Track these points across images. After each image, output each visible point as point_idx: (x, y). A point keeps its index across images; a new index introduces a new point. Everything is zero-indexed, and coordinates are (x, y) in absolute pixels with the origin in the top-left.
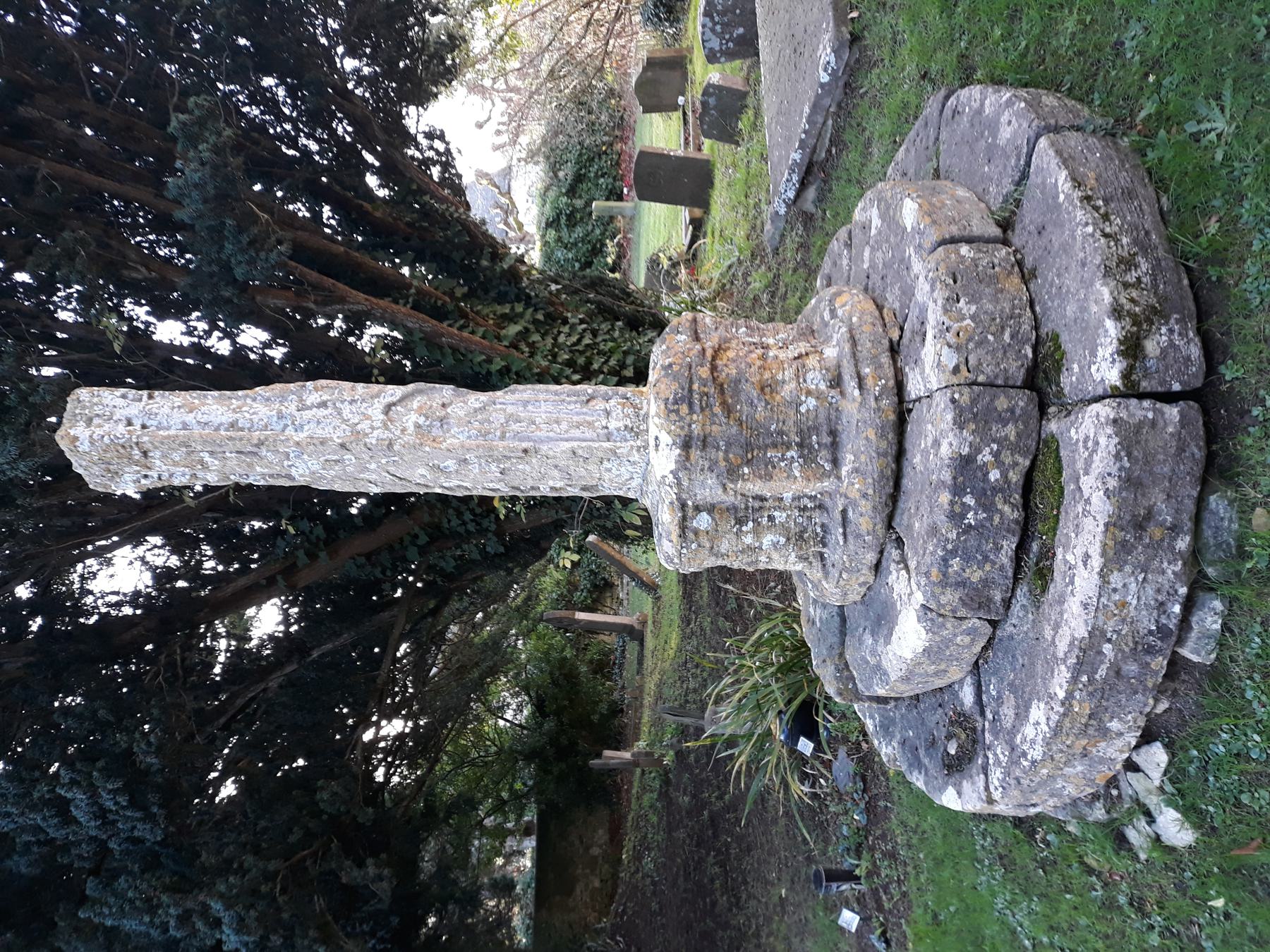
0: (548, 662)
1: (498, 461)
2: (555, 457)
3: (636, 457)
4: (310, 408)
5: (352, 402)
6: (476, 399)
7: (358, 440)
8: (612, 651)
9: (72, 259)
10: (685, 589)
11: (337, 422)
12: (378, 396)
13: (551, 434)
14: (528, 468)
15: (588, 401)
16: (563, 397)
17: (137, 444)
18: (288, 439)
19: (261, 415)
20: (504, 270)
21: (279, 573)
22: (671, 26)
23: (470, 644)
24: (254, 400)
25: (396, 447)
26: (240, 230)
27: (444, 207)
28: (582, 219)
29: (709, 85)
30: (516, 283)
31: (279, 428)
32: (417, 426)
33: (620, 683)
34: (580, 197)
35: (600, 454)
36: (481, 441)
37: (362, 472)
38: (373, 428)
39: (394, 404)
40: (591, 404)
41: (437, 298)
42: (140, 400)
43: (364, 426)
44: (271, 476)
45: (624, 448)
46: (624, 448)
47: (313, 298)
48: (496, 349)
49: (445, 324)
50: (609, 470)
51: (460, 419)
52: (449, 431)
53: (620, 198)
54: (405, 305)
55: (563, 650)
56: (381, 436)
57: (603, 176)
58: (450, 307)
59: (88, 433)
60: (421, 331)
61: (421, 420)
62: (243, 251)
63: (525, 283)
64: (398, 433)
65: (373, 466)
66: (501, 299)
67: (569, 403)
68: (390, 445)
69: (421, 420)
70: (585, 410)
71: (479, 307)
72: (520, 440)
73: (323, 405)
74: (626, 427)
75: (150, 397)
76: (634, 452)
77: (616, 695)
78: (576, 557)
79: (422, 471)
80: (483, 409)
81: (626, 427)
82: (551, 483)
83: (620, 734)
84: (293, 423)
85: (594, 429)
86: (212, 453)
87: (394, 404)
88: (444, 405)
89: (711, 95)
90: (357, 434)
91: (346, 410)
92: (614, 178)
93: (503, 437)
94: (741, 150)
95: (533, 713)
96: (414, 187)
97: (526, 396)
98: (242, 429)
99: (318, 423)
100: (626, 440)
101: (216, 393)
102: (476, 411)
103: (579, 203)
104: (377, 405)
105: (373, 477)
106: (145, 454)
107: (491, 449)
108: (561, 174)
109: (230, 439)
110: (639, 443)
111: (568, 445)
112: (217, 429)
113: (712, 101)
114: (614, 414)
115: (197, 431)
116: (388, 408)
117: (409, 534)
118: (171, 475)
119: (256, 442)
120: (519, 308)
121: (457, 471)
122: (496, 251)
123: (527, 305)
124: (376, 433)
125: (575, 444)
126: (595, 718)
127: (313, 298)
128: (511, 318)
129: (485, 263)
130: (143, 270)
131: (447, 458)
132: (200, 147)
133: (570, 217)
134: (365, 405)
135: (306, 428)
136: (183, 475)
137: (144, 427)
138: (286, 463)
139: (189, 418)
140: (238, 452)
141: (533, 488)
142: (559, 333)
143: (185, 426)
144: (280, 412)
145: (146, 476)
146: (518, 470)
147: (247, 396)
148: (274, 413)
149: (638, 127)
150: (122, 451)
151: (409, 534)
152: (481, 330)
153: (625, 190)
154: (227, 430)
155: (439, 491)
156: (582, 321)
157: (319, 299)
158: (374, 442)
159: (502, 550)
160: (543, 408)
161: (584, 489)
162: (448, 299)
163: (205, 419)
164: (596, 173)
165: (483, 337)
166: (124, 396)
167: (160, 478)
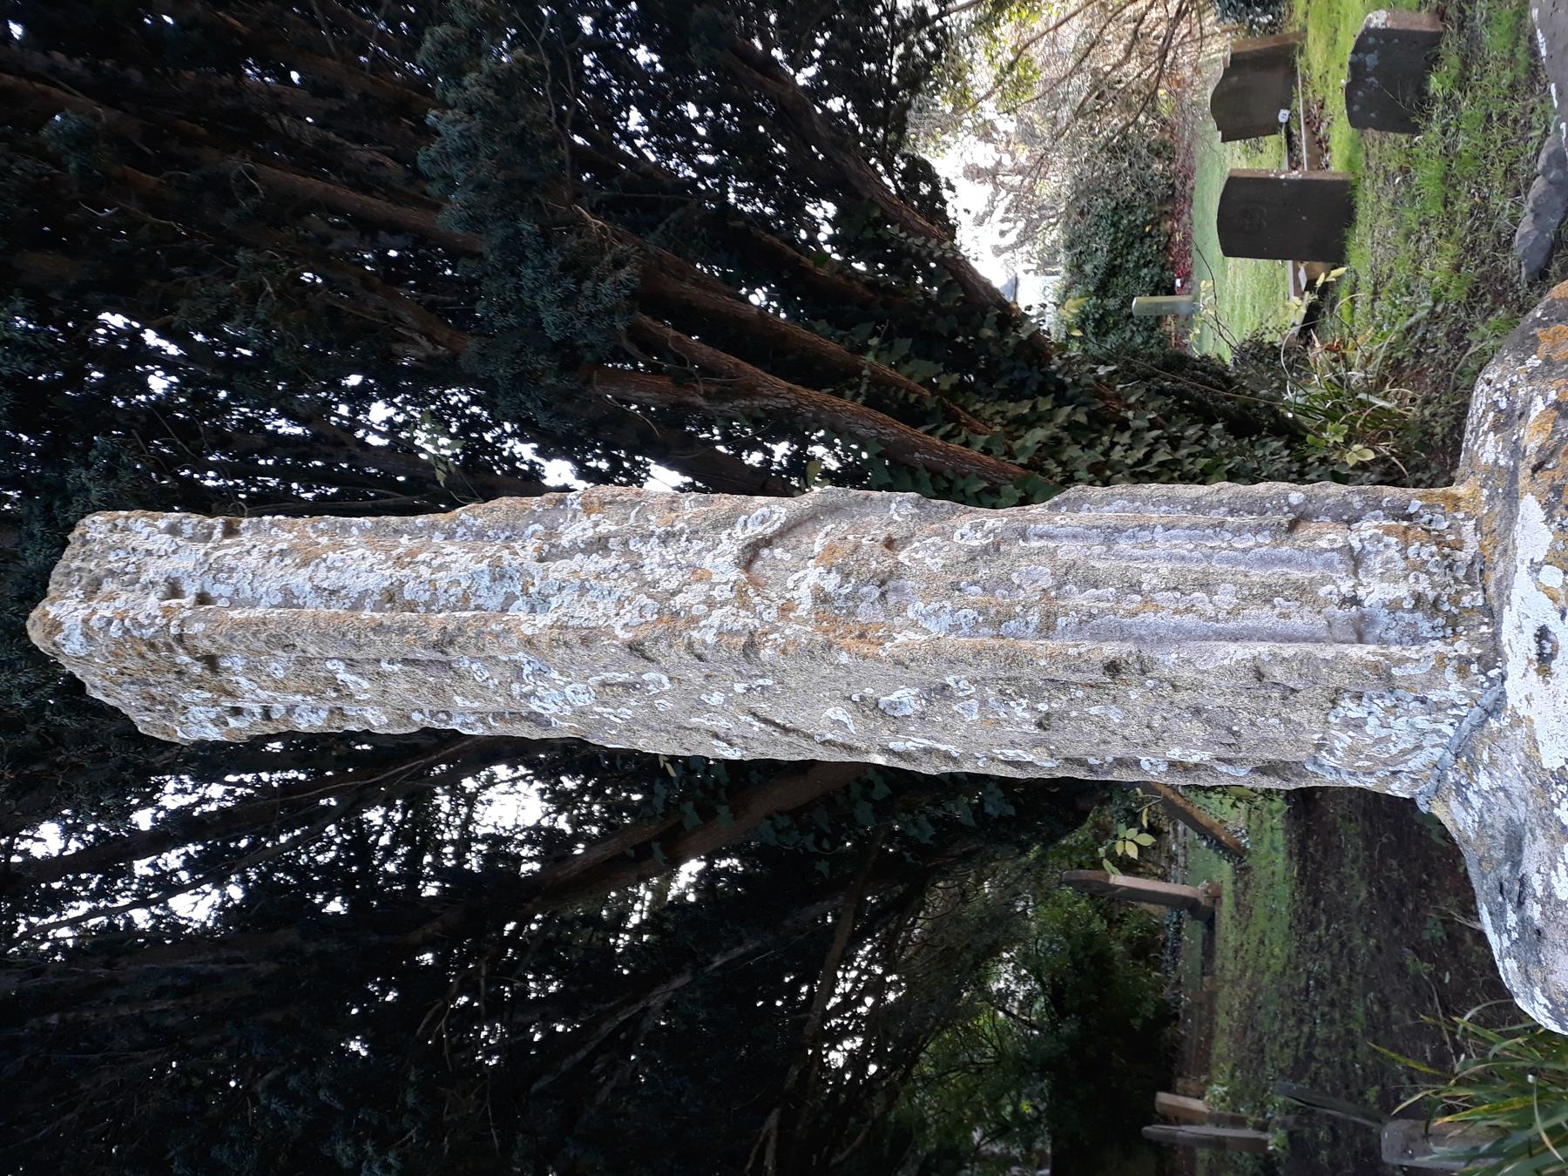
0: (1068, 937)
1: (1035, 693)
2: (1195, 686)
3: (1453, 689)
4: (567, 554)
5: (665, 540)
6: (971, 527)
7: (672, 634)
8: (1161, 928)
9: (253, 300)
10: (1303, 868)
11: (626, 588)
12: (729, 521)
13: (1189, 620)
14: (1115, 716)
15: (1293, 526)
16: (1215, 516)
17: (180, 639)
18: (508, 631)
19: (454, 573)
20: (1021, 342)
21: (656, 839)
22: (1265, 12)
23: (958, 920)
24: (450, 536)
25: (766, 653)
26: (547, 240)
27: (920, 241)
28: (1116, 324)
29: (1368, 32)
30: (1041, 366)
31: (495, 602)
32: (822, 598)
33: (1173, 975)
34: (1114, 295)
35: (1338, 680)
36: (985, 638)
37: (692, 712)
38: (711, 604)
39: (768, 542)
40: (1305, 532)
41: (909, 391)
42: (208, 537)
43: (690, 598)
44: (498, 716)
45: (1414, 662)
46: (1414, 662)
47: (701, 388)
48: (1005, 471)
49: (920, 431)
50: (1359, 725)
51: (931, 578)
52: (901, 610)
53: (1171, 291)
54: (853, 400)
55: (1090, 921)
56: (730, 624)
57: (1146, 265)
58: (930, 404)
59: (82, 613)
60: (879, 441)
61: (831, 582)
62: (554, 281)
63: (1055, 364)
64: (771, 615)
65: (717, 699)
66: (1015, 393)
67: (1238, 531)
68: (751, 647)
69: (831, 582)
70: (1285, 550)
71: (978, 406)
72: (1095, 636)
73: (599, 545)
74: (1418, 598)
75: (230, 531)
76: (1450, 675)
77: (1167, 993)
78: (1147, 840)
79: (838, 712)
80: (993, 550)
81: (1418, 598)
82: (1175, 753)
83: (1174, 1049)
84: (525, 591)
85: (1318, 606)
86: (351, 664)
87: (768, 542)
88: (890, 543)
89: (1370, 50)
90: (674, 620)
91: (653, 557)
92: (1163, 267)
93: (1047, 628)
94: (1430, 137)
95: (1047, 1006)
96: (877, 214)
97: (1109, 515)
98: (411, 606)
99: (583, 590)
100: (1417, 639)
101: (368, 521)
102: (973, 555)
103: (1112, 303)
104: (726, 545)
105: (721, 724)
106: (211, 662)
107: (1013, 660)
108: (1088, 268)
109: (379, 628)
110: (1461, 647)
111: (1240, 652)
112: (357, 606)
113: (1371, 60)
114: (1375, 563)
115: (314, 608)
116: (751, 554)
117: (858, 780)
118: (290, 710)
119: (434, 636)
120: (1045, 404)
121: (922, 716)
122: (1007, 315)
123: (1059, 402)
124: (717, 614)
125: (1263, 649)
126: (1137, 1023)
127: (701, 388)
128: (1026, 423)
129: (988, 332)
130: (424, 342)
131: (896, 683)
132: (466, 82)
133: (1099, 323)
134: (697, 545)
135: (554, 602)
136: (314, 710)
137: (203, 599)
138: (516, 687)
139: (299, 580)
140: (405, 661)
141: (1120, 762)
142: (1113, 444)
143: (289, 598)
144: (496, 563)
145: (237, 712)
146: (1087, 719)
147: (434, 526)
148: (484, 565)
149: (1196, 196)
150: (151, 656)
151: (858, 780)
152: (981, 440)
153: (1178, 283)
154: (378, 607)
155: (880, 760)
156: (1153, 425)
157: (713, 389)
158: (710, 638)
159: (1011, 811)
160: (1161, 544)
161: (1266, 769)
162: (926, 392)
163: (329, 580)
164: (1137, 262)
165: (987, 451)
166: (173, 530)
167: (267, 714)
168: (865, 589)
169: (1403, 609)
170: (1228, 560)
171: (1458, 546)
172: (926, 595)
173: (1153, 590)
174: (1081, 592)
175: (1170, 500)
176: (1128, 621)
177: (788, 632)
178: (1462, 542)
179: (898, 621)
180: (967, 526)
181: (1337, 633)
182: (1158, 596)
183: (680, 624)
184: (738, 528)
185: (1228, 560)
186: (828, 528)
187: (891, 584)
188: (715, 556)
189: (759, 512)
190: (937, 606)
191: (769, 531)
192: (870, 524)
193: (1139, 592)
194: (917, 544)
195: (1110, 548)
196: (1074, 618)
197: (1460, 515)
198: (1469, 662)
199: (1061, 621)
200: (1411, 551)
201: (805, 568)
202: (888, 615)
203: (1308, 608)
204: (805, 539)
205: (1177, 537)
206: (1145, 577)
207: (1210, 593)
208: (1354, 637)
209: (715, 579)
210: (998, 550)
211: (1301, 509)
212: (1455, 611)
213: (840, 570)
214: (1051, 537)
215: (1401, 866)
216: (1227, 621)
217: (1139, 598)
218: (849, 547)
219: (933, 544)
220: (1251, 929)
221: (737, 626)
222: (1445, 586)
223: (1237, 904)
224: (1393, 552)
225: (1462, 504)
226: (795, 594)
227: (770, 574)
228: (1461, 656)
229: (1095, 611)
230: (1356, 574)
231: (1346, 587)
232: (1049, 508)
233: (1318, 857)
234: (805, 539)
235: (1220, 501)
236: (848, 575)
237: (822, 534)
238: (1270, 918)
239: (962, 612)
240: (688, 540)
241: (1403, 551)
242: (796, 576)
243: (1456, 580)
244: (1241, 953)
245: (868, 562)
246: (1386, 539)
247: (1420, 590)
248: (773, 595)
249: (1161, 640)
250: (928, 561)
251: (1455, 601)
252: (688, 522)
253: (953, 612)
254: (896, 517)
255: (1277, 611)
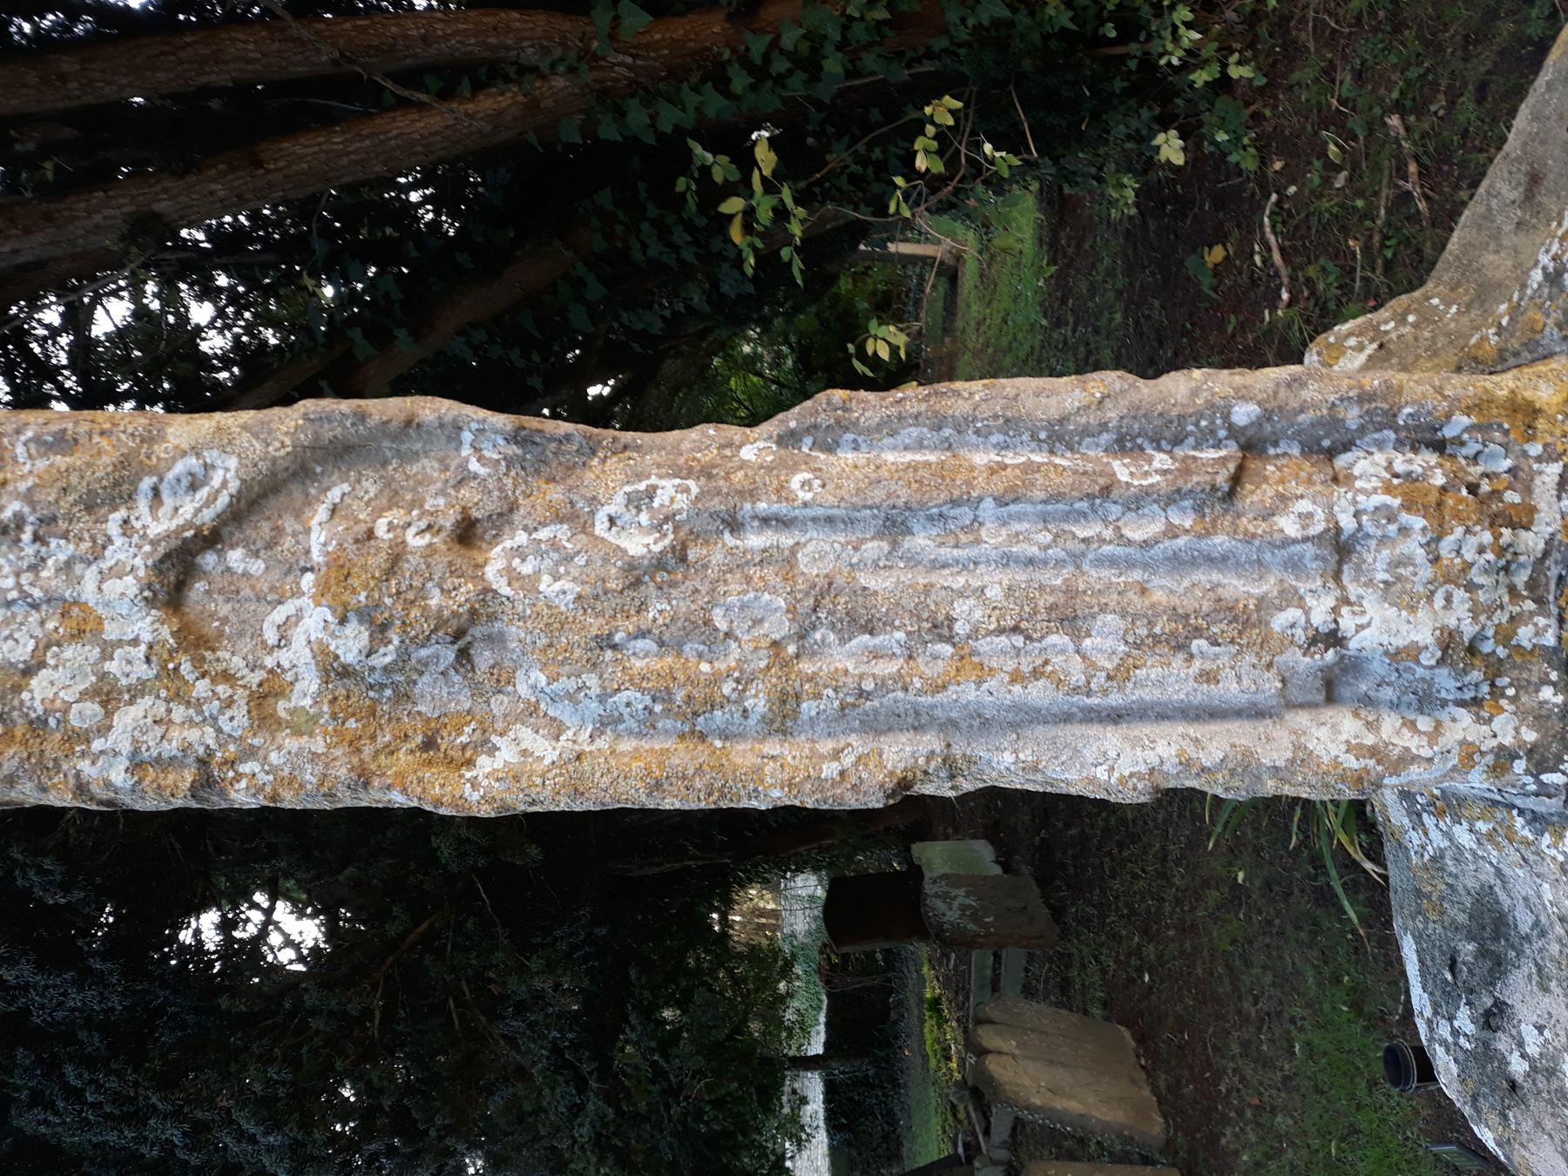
12: (117, 491)
13: (1038, 693)
38: (107, 695)
39: (211, 538)
51: (556, 623)
52: (502, 680)
56: (152, 745)
61: (351, 644)
64: (237, 720)
69: (351, 644)
70: (1221, 541)
74: (1448, 641)
87: (211, 538)
102: (636, 575)
104: (119, 551)
114: (1378, 562)
116: (177, 572)
124: (127, 718)
134: (60, 550)
168: (424, 652)
169: (1418, 663)
170: (1112, 562)
171: (1522, 519)
172: (553, 659)
173: (974, 634)
174: (843, 641)
175: (1011, 427)
176: (926, 700)
177: (274, 757)
178: (1533, 510)
179: (499, 704)
180: (620, 499)
181: (1295, 695)
182: (983, 645)
183: (52, 748)
184: (143, 505)
185: (1112, 562)
186: (335, 494)
187: (477, 631)
188: (103, 577)
189: (179, 468)
190: (572, 684)
191: (208, 515)
192: (425, 481)
193: (949, 639)
194: (521, 538)
195: (895, 545)
196: (830, 701)
197: (1535, 449)
198: (1514, 756)
199: (808, 708)
200: (1446, 546)
201: (297, 593)
202: (477, 690)
203: (1250, 658)
204: (289, 524)
205: (1020, 517)
206: (960, 608)
207: (1077, 635)
208: (1321, 697)
209: (111, 632)
210: (683, 559)
211: (1251, 432)
212: (1502, 652)
213: (365, 615)
214: (784, 523)
215: (1163, 307)
216: (1105, 692)
217: (947, 650)
218: (378, 562)
219: (554, 544)
220: (995, 305)
221: (171, 748)
222: (1490, 610)
223: (982, 276)
224: (1414, 547)
225: (1541, 424)
226: (284, 657)
227: (225, 609)
228: (1501, 747)
229: (868, 685)
230: (1337, 576)
231: (1320, 617)
232: (781, 441)
233: (1070, 250)
234: (289, 524)
235: (1104, 427)
236: (384, 627)
237: (322, 512)
238: (1015, 299)
239: (624, 696)
240: (36, 538)
241: (1432, 546)
242: (279, 614)
243: (1512, 590)
244: (983, 328)
245: (422, 593)
246: (1405, 518)
247: (1453, 623)
248: (237, 662)
249: (986, 724)
250: (546, 585)
251: (1505, 636)
252: (28, 497)
253: (602, 699)
254: (474, 466)
255: (1197, 664)
